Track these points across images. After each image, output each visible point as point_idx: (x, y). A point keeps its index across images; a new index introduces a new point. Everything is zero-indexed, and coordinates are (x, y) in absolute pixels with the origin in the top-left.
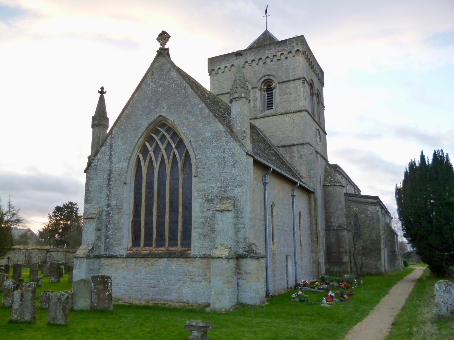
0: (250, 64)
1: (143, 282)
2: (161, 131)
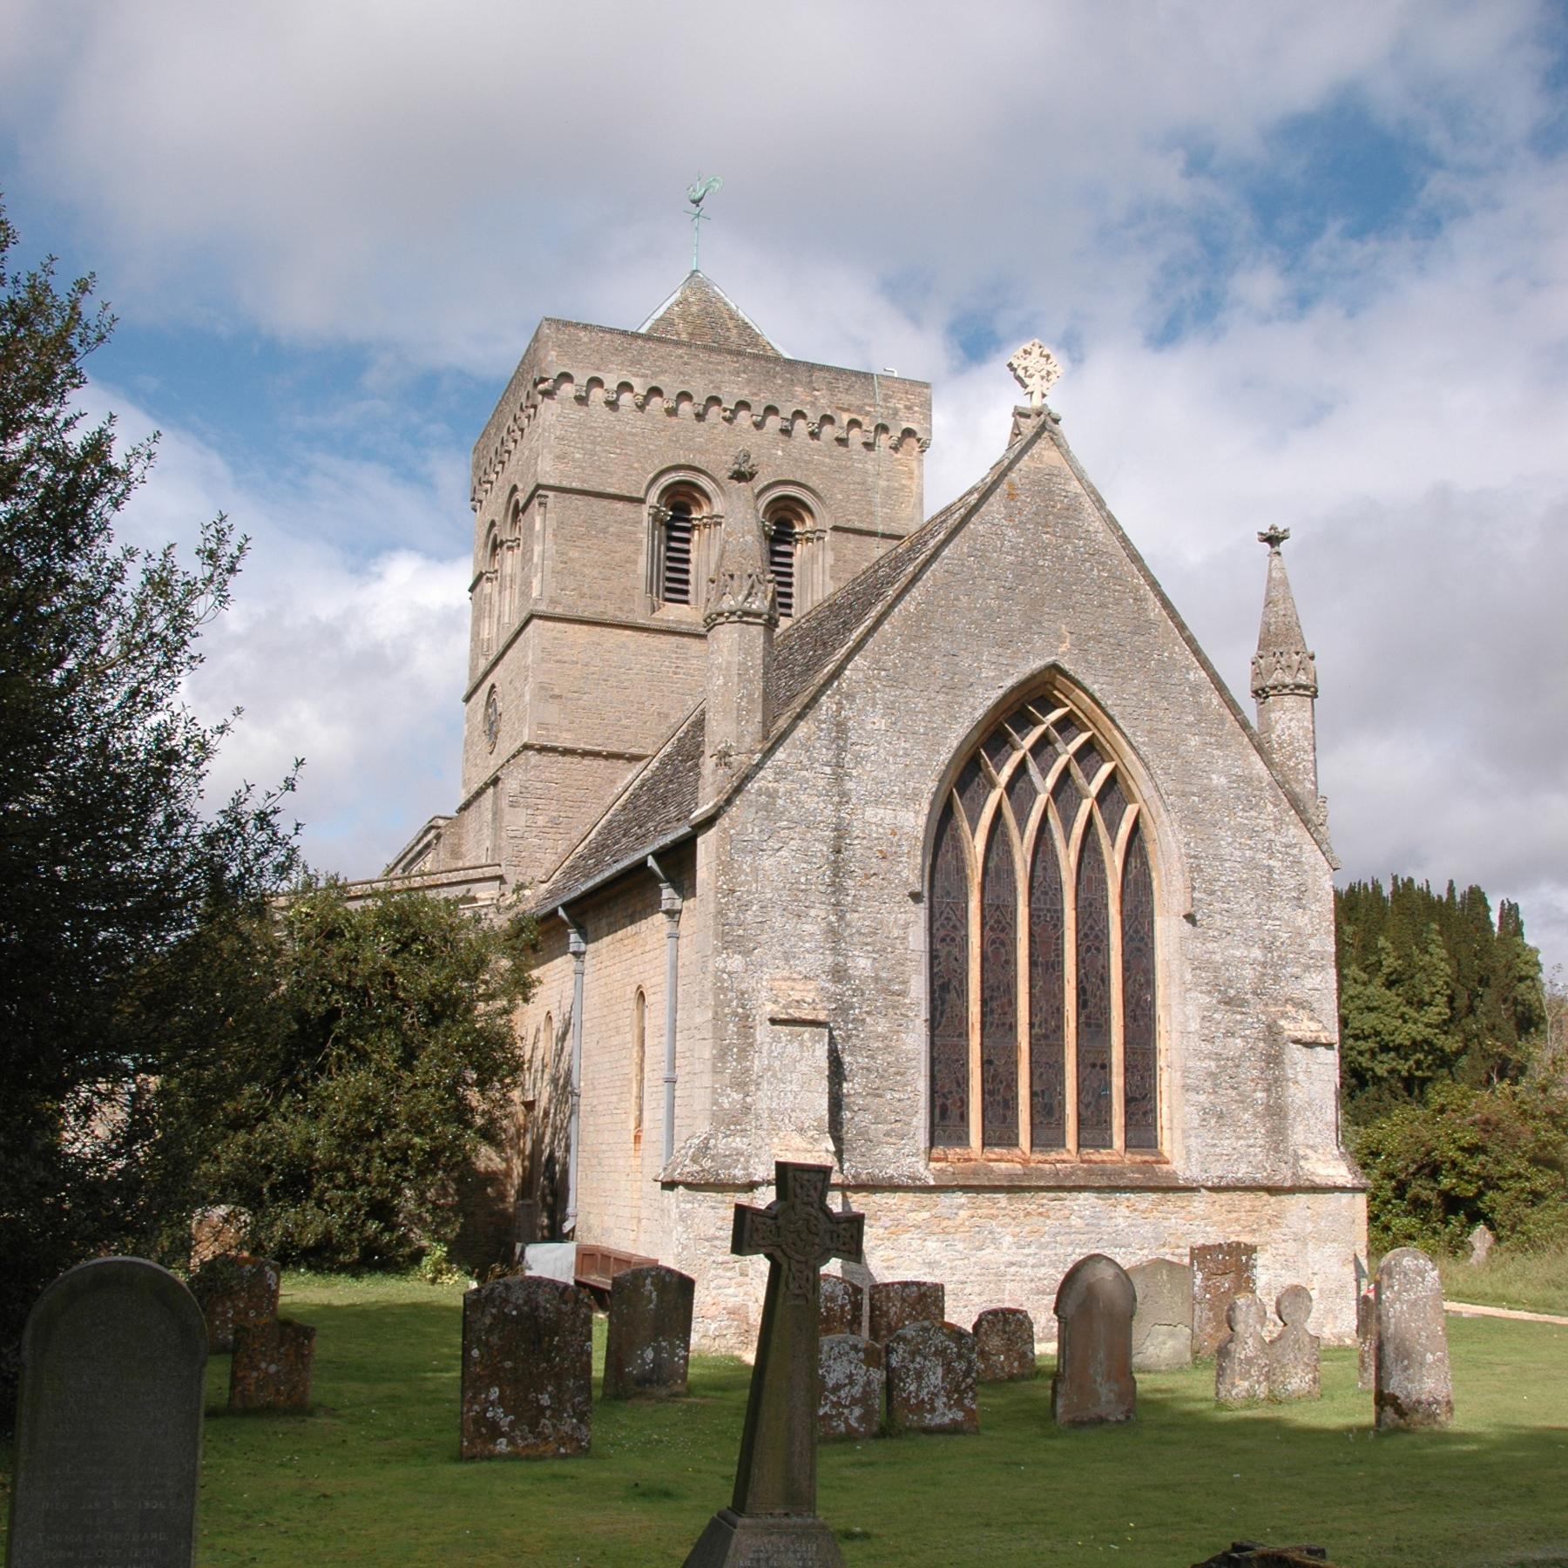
1: (1009, 1277)
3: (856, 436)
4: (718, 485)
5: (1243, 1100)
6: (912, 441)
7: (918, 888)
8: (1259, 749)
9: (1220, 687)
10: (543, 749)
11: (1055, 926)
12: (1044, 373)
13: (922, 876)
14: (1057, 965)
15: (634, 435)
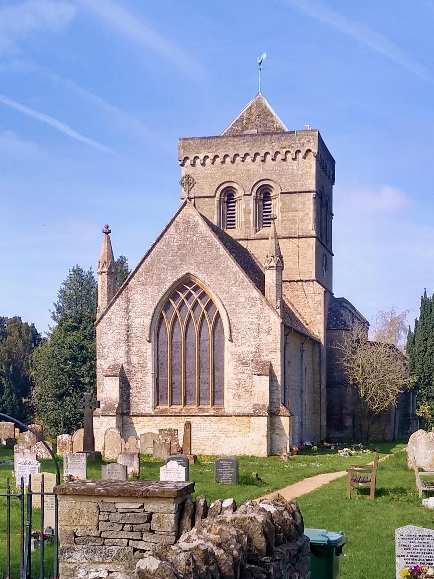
2: (188, 289)
15: (211, 174)
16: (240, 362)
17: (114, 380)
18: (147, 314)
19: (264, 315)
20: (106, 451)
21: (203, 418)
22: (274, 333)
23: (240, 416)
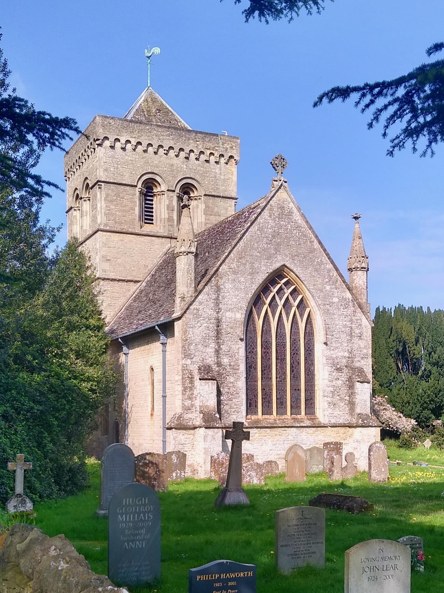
0: (166, 152)
3: (212, 159)
4: (163, 179)
5: (341, 399)
6: (233, 160)
7: (242, 337)
8: (349, 289)
9: (337, 269)
10: (104, 279)
11: (284, 347)
12: (282, 165)
13: (244, 334)
14: (284, 359)
15: (132, 161)
16: (334, 368)
17: (210, 384)
18: (240, 307)
19: (356, 318)
20: (372, 471)
21: (299, 429)
22: (366, 338)
23: (336, 427)
